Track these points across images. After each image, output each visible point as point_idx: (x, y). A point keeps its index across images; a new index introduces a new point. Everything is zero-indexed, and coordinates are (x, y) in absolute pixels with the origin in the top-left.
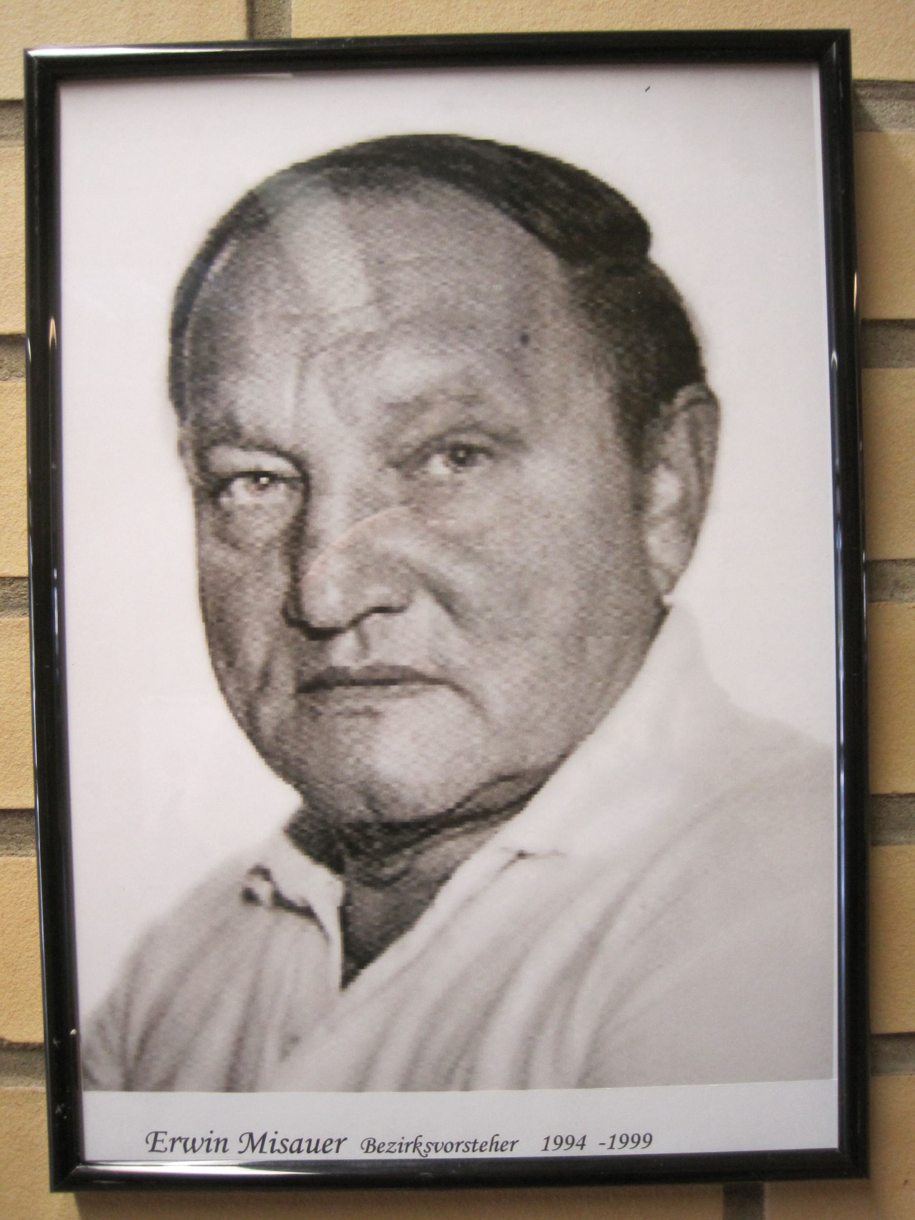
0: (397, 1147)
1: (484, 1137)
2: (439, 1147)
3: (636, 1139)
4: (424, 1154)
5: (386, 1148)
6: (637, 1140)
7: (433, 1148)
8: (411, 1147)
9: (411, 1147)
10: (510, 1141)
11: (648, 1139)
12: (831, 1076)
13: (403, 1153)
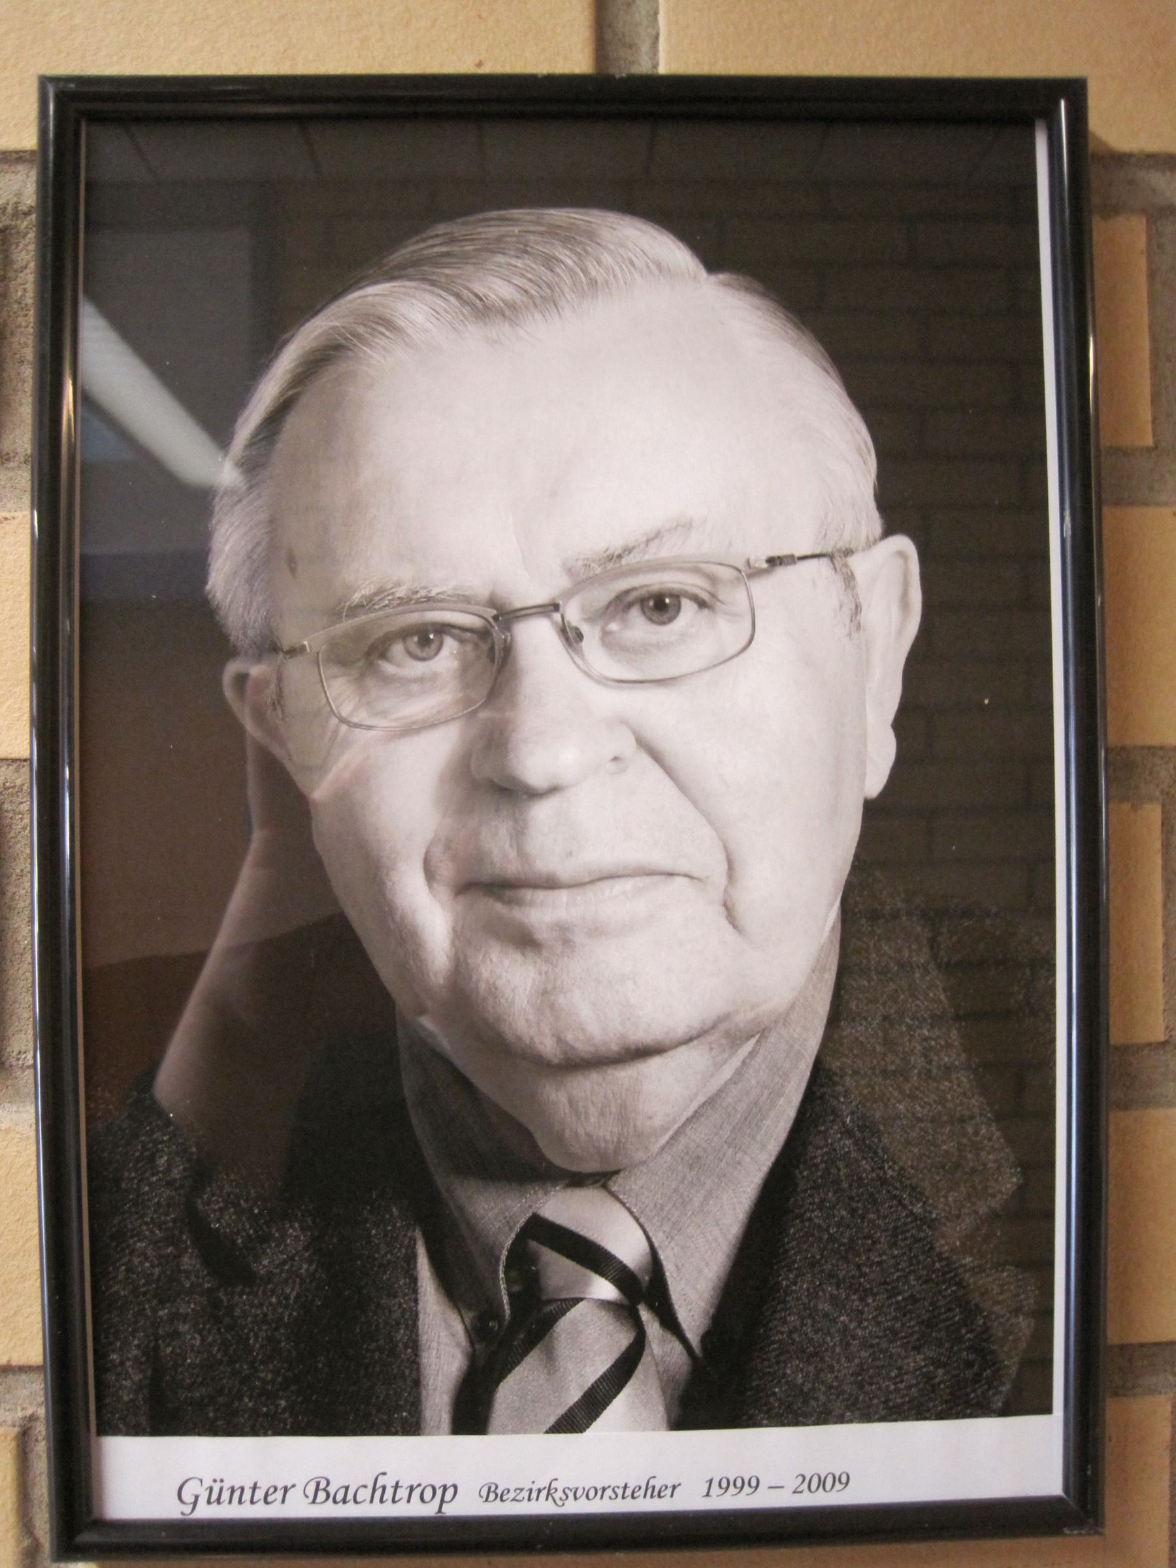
0: (525, 1494)
1: (636, 1479)
2: (579, 1493)
3: (739, 1484)
4: (560, 1503)
5: (512, 1495)
6: (740, 1484)
7: (571, 1495)
8: (544, 1494)
9: (544, 1494)
10: (599, 1487)
11: (754, 1483)
12: (1048, 1410)
13: (225, 1504)
